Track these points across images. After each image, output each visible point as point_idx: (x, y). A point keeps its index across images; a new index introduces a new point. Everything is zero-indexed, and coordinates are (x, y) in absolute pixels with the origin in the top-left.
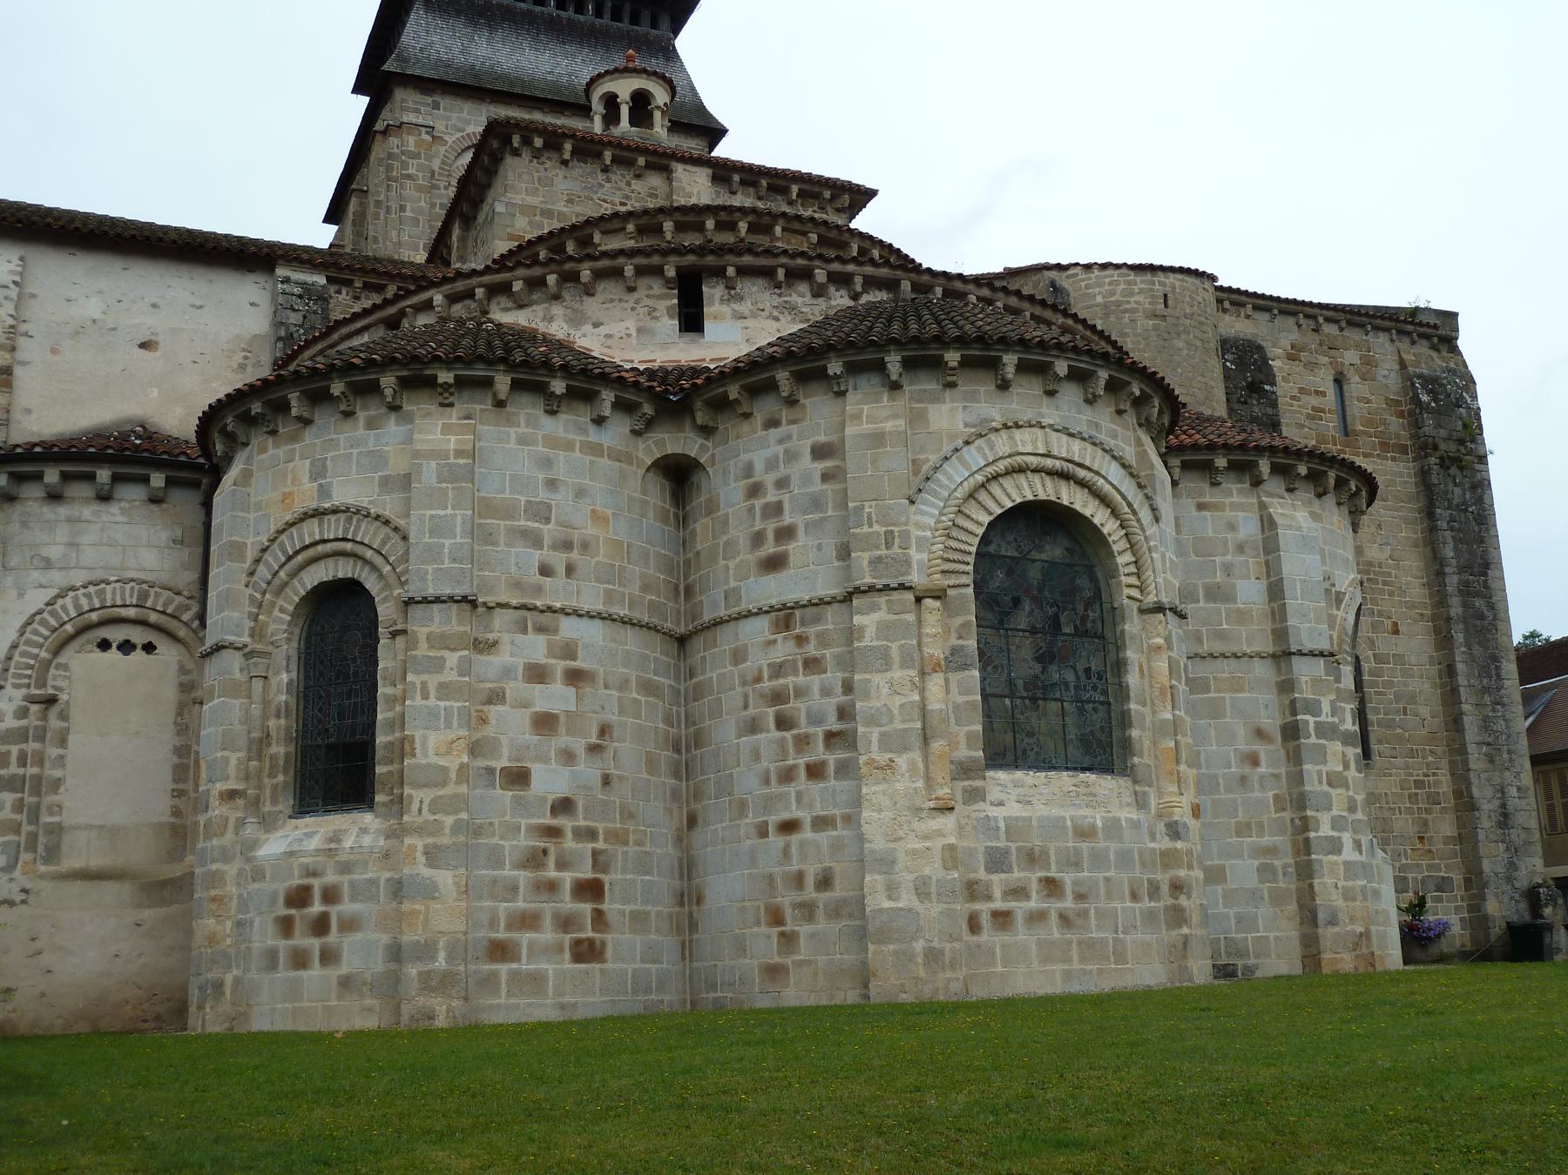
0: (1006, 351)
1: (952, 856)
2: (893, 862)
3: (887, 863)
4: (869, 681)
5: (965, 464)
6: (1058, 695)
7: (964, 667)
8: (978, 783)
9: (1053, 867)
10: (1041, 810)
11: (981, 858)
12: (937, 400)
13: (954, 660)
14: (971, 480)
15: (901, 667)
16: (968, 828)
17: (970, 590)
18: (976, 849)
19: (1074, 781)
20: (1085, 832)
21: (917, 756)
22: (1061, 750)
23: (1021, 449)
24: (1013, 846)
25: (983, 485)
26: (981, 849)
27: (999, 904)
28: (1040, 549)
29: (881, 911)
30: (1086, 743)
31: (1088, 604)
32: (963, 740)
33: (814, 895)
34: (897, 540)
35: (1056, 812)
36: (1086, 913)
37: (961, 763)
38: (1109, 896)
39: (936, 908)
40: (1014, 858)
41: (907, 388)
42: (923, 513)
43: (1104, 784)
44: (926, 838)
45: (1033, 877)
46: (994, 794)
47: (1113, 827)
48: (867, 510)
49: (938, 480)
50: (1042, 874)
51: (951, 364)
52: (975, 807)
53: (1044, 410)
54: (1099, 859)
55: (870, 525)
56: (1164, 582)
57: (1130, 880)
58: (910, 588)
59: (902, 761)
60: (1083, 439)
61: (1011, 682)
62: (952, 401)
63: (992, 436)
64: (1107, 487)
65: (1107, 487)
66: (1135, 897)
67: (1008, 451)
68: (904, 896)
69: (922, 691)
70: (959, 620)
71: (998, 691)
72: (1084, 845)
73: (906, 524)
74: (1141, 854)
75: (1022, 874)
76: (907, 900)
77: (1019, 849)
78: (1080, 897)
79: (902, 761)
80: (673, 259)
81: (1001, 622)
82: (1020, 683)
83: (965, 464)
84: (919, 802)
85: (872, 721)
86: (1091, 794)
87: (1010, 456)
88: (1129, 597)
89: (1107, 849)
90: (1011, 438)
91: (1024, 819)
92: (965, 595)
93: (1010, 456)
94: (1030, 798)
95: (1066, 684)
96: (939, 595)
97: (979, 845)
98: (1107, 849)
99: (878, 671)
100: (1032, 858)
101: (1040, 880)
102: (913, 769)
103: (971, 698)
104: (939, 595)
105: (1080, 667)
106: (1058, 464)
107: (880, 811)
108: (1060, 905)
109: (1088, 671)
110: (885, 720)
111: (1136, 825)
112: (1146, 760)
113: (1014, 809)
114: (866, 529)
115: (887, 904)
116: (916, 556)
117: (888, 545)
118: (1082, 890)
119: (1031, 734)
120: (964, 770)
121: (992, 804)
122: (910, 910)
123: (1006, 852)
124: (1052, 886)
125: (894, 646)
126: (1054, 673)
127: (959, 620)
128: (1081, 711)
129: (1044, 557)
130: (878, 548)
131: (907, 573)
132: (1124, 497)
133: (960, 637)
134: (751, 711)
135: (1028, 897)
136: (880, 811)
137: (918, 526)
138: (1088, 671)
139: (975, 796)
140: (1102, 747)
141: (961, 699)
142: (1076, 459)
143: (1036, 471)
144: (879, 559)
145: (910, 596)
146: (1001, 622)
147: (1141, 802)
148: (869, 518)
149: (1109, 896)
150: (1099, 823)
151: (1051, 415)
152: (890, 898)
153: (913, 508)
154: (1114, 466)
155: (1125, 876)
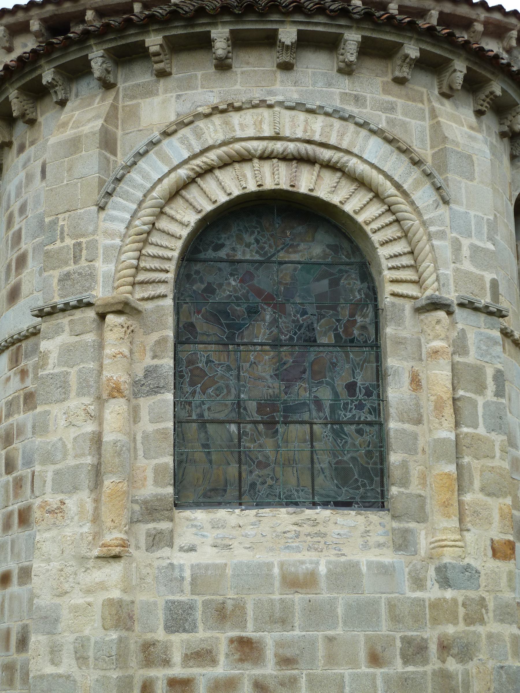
0: (214, 24)
1: (121, 616)
2: (57, 620)
3: (50, 621)
4: (48, 413)
5: (164, 158)
6: (306, 417)
7: (156, 390)
8: (164, 525)
9: (250, 625)
10: (241, 555)
11: (161, 615)
12: (150, 93)
13: (144, 385)
14: (173, 175)
15: (78, 395)
16: (149, 580)
17: (169, 302)
18: (155, 604)
19: (295, 518)
20: (299, 581)
21: (85, 496)
22: (306, 480)
23: (239, 134)
24: (199, 600)
25: (193, 181)
26: (161, 603)
27: (178, 671)
28: (292, 247)
29: (42, 677)
30: (342, 473)
31: (357, 307)
32: (150, 475)
33: (15, 656)
34: (84, 252)
35: (261, 557)
36: (293, 681)
37: (145, 502)
38: (331, 659)
39: (92, 675)
40: (199, 614)
41: (121, 86)
42: (113, 219)
43: (350, 520)
44: (89, 591)
45: (222, 638)
46: (185, 536)
47: (345, 575)
48: (61, 223)
49: (132, 180)
50: (235, 633)
51: (152, 49)
52: (159, 553)
53: (278, 87)
54: (318, 615)
55: (62, 240)
56: (449, 272)
57: (368, 639)
58: (89, 305)
59: (72, 503)
60: (327, 114)
61: (239, 404)
62: (166, 91)
63: (201, 124)
64: (220, 151)
65: (220, 151)
66: (375, 659)
67: (220, 137)
68: (65, 660)
69: (99, 419)
70: (155, 337)
71: (221, 416)
72: (297, 597)
73: (95, 232)
74: (391, 606)
75: (209, 634)
76: (67, 665)
77: (206, 604)
78: (286, 661)
79: (72, 503)
80: (34, 12)
81: (231, 338)
82: (252, 406)
83: (164, 158)
84: (84, 551)
85: (48, 458)
86: (319, 534)
87: (224, 143)
88: (394, 295)
89: (332, 603)
90: (227, 123)
91: (216, 566)
92: (159, 309)
93: (224, 143)
94: (235, 543)
95: (318, 403)
96: (124, 308)
97: (153, 598)
98: (332, 603)
99: (56, 402)
100: (222, 614)
101: (232, 641)
102: (81, 512)
103: (162, 425)
104: (124, 308)
105: (340, 384)
106: (291, 147)
107: (48, 561)
108: (257, 672)
109: (351, 387)
110: (59, 456)
111: (385, 571)
112: (414, 488)
113: (207, 555)
114: (58, 244)
115: (49, 670)
116: (104, 268)
117: (76, 259)
118: (288, 653)
119: (261, 465)
120: (151, 510)
121: (181, 549)
122: (68, 677)
123: (191, 607)
124: (246, 649)
125: (73, 371)
126: (302, 392)
127: (155, 337)
128: (338, 434)
129: (295, 257)
130: (66, 264)
131: (90, 288)
132: (388, 177)
133: (154, 357)
134: (370, 448)
135: (214, 662)
136: (48, 561)
137: (107, 234)
138: (351, 387)
139: (158, 541)
140: (361, 480)
141: (151, 428)
142: (317, 138)
143: (264, 157)
144: (67, 276)
145: (91, 314)
146: (231, 338)
147: (403, 542)
148: (62, 233)
149: (331, 659)
150: (323, 569)
151: (284, 89)
152: (53, 663)
153: (103, 215)
154: (375, 141)
155: (360, 636)
